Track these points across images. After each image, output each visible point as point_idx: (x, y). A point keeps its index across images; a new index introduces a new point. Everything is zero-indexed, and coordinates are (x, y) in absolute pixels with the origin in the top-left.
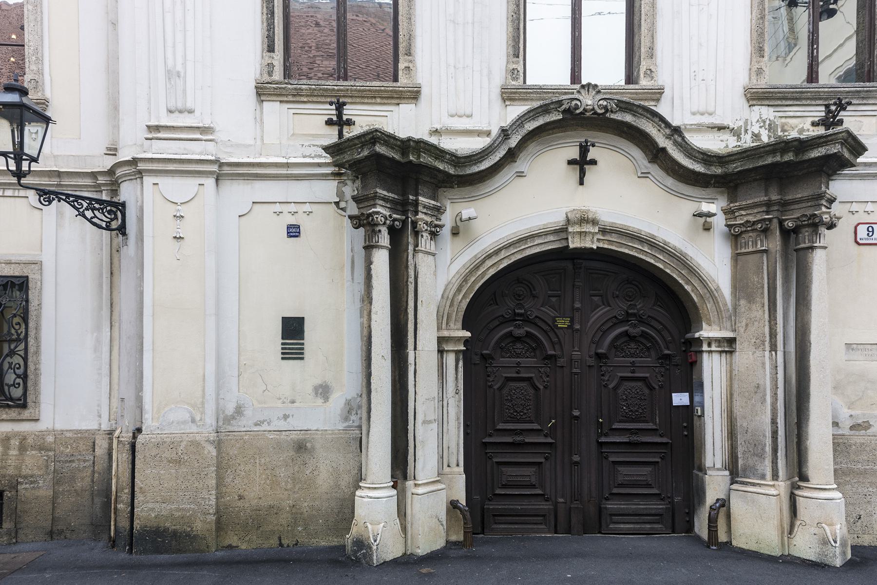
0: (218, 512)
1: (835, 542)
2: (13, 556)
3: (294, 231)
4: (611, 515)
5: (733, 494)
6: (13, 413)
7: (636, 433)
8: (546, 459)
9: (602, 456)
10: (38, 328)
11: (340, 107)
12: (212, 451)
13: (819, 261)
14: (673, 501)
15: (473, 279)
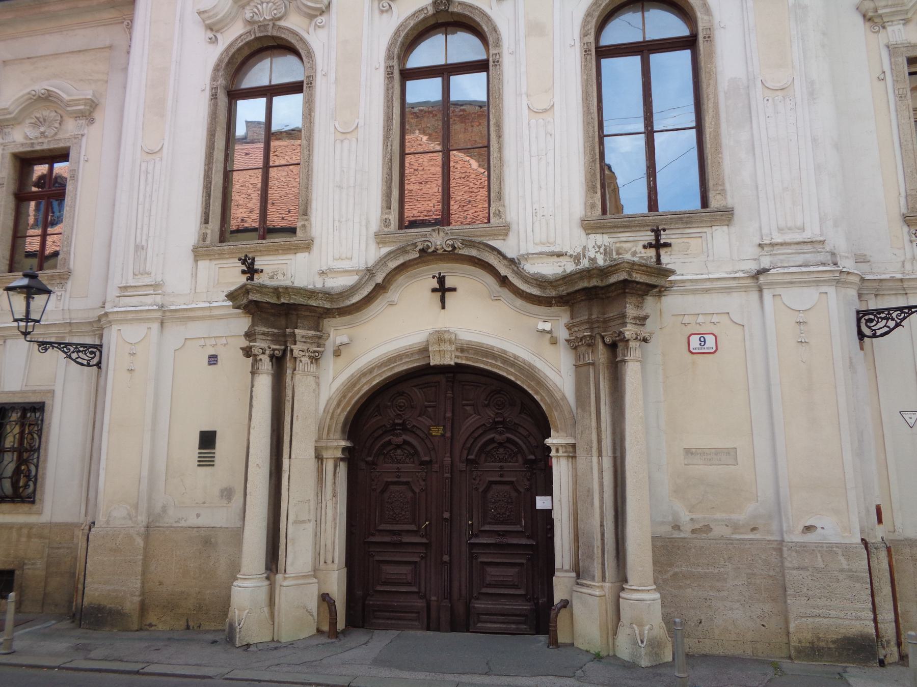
0: (143, 593)
1: (642, 642)
2: (144, 665)
3: (213, 360)
4: (479, 614)
5: (575, 594)
6: (25, 507)
7: (503, 535)
8: (422, 558)
9: (472, 557)
10: (47, 442)
11: (657, 232)
12: (140, 542)
13: (632, 373)
14: (538, 603)
15: (350, 394)
